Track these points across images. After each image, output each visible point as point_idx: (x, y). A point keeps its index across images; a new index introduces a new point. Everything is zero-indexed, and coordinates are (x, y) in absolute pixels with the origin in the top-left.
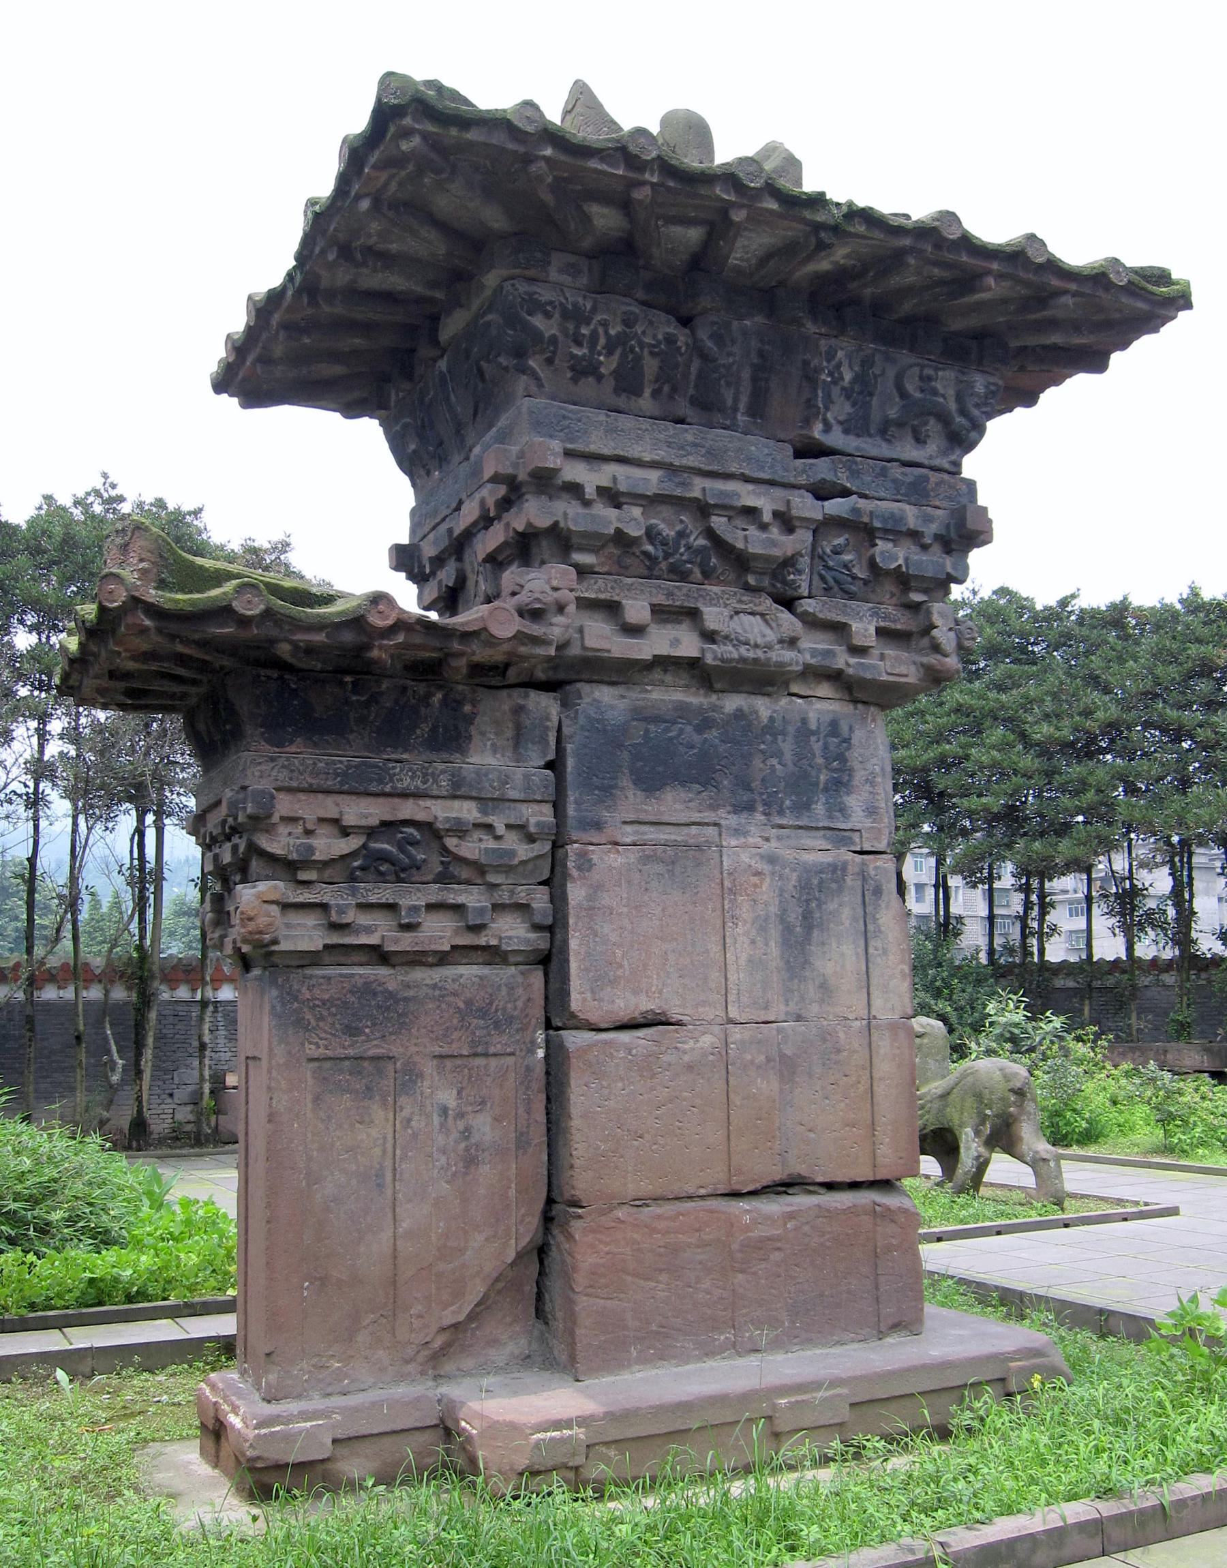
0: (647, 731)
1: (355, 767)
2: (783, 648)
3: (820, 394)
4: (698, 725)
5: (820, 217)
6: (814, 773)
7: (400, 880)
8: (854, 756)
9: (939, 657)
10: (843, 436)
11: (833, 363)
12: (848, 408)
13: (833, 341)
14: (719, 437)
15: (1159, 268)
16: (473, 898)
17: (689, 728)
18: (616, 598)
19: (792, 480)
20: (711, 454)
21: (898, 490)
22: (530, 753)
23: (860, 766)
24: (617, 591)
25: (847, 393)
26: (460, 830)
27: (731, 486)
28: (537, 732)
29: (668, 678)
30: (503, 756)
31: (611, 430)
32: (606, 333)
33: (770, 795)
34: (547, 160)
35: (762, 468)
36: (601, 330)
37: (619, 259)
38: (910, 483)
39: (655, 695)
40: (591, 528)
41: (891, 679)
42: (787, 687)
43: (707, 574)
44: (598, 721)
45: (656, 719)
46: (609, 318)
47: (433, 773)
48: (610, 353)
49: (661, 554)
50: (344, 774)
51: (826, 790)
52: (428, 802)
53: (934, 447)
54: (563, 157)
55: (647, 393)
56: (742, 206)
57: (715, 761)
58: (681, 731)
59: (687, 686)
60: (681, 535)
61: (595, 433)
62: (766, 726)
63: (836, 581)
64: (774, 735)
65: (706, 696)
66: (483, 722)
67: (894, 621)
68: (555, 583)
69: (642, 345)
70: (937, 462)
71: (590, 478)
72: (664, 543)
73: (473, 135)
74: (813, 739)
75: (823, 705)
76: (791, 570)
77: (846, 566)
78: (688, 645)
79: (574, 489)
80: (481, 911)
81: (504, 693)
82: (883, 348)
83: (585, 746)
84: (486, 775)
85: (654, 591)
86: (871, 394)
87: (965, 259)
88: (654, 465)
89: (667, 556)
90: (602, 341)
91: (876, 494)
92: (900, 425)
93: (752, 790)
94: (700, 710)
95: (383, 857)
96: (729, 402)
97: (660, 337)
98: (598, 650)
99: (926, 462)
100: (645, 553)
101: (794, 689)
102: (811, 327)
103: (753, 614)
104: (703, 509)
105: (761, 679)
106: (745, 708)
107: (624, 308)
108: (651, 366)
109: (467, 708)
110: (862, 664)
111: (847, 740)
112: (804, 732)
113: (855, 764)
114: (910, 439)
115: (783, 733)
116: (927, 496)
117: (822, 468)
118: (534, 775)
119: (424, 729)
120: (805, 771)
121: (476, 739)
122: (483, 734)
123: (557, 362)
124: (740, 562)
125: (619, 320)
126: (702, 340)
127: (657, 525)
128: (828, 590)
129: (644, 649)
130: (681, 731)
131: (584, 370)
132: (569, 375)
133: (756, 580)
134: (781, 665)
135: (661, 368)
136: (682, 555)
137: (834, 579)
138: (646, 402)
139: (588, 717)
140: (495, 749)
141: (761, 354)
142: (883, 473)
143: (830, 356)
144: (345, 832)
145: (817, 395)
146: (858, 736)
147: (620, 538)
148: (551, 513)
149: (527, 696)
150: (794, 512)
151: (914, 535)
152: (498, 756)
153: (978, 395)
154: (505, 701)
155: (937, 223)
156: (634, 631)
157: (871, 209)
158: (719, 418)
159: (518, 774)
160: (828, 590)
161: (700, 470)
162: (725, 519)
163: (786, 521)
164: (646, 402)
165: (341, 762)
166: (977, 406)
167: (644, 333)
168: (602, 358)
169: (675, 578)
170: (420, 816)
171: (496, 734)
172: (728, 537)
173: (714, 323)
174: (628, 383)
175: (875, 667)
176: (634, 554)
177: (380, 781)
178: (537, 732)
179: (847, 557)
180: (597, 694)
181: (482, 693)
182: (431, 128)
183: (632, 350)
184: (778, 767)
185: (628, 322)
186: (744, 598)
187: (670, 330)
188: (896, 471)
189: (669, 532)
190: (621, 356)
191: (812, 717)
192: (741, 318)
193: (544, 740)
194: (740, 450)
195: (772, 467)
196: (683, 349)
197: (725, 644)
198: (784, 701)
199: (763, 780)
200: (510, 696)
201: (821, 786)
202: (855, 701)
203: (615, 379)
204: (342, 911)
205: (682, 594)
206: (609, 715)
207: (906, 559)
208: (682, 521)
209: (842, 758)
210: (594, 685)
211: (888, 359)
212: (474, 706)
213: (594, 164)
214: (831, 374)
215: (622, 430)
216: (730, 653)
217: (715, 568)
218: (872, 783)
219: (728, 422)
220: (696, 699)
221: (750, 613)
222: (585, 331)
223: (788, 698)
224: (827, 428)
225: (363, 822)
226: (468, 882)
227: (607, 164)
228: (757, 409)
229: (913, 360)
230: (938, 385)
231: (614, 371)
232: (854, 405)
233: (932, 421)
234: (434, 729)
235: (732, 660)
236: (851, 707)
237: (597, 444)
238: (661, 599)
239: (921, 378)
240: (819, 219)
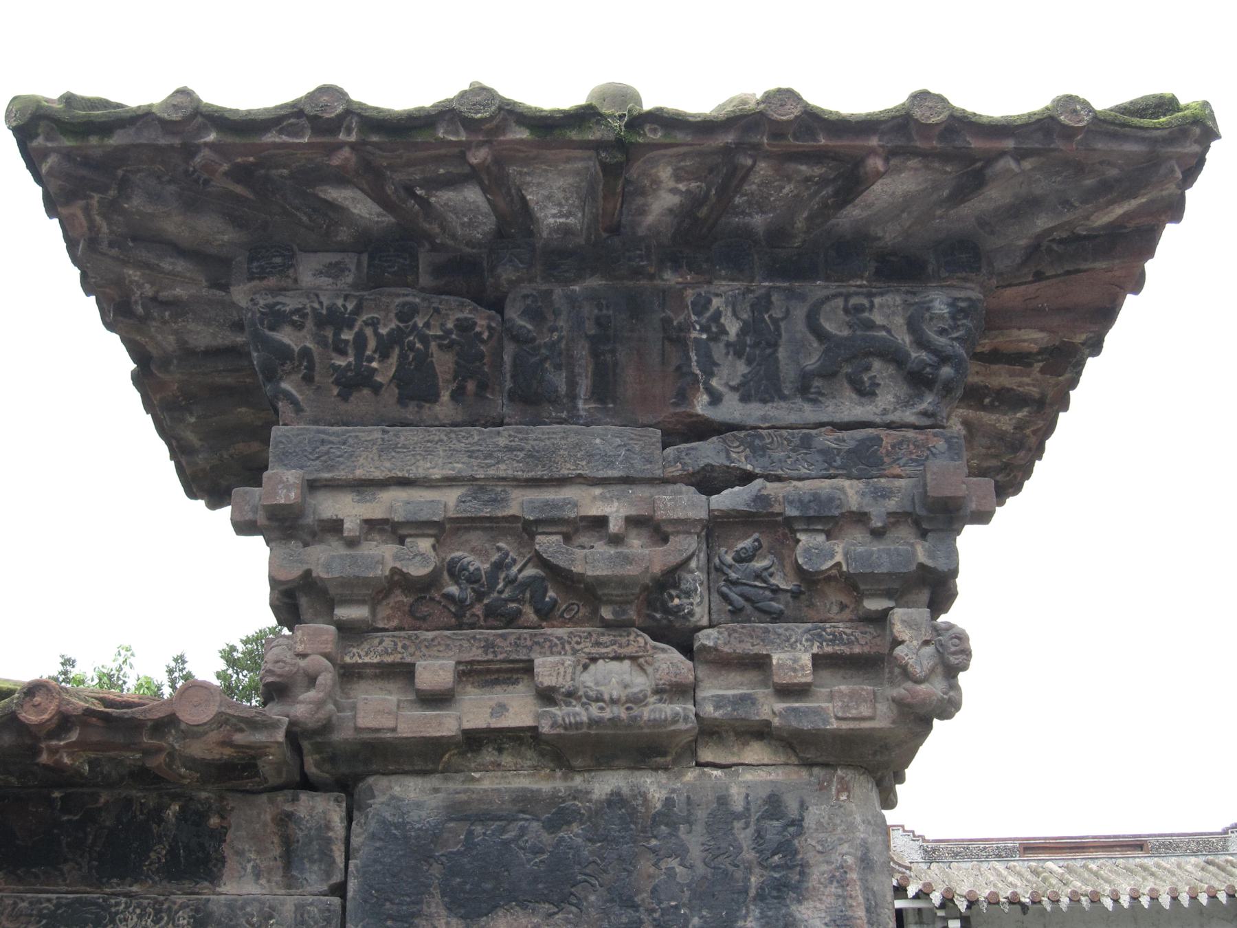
0: (470, 833)
1: (67, 905)
2: (660, 701)
3: (694, 358)
4: (549, 820)
5: (595, 134)
6: (739, 874)
8: (809, 845)
9: (909, 684)
10: (740, 406)
11: (708, 315)
12: (742, 368)
13: (703, 290)
15: (1154, 96)
17: (535, 825)
18: (408, 660)
19: (658, 473)
20: (533, 457)
21: (830, 463)
22: (307, 875)
23: (820, 858)
24: (412, 650)
25: (737, 349)
27: (568, 493)
28: (315, 846)
29: (506, 759)
30: (269, 881)
31: (386, 449)
32: (376, 333)
33: (664, 912)
34: (210, 145)
35: (610, 464)
36: (369, 332)
38: (849, 451)
39: (486, 784)
40: (350, 572)
41: (845, 726)
42: (694, 753)
43: (546, 613)
44: (397, 826)
45: (483, 817)
47: (169, 908)
48: (384, 356)
49: (470, 594)
51: (761, 897)
53: (890, 398)
54: (230, 139)
55: (445, 396)
56: (480, 145)
57: (577, 868)
58: (523, 830)
59: (535, 768)
60: (499, 566)
61: (364, 454)
62: (659, 813)
63: (747, 599)
64: (673, 826)
65: (565, 778)
66: (237, 839)
67: (850, 643)
68: (300, 648)
69: (425, 340)
70: (895, 417)
71: (350, 510)
72: (473, 579)
73: (116, 140)
74: (738, 825)
75: (755, 773)
76: (674, 593)
77: (758, 576)
78: (518, 709)
79: (335, 527)
82: (786, 284)
83: (376, 861)
84: (243, 908)
85: (466, 644)
86: (774, 345)
87: (823, 142)
88: (450, 481)
89: (480, 596)
90: (372, 344)
91: (794, 473)
92: (829, 374)
93: (635, 907)
94: (554, 798)
96: (563, 389)
97: (450, 325)
98: (378, 730)
99: (878, 420)
100: (449, 597)
101: (706, 755)
103: (618, 658)
104: (527, 529)
105: (645, 749)
106: (625, 791)
107: (398, 301)
108: (443, 362)
109: (214, 821)
110: (794, 710)
111: (798, 823)
112: (723, 815)
113: (812, 857)
114: (848, 392)
115: (689, 821)
116: (879, 463)
117: (708, 452)
118: (311, 904)
119: (159, 852)
120: (726, 873)
121: (232, 863)
122: (240, 853)
123: (317, 379)
124: (586, 593)
125: (392, 315)
126: (510, 320)
127: (460, 559)
128: (736, 612)
129: (446, 724)
130: (523, 830)
131: (355, 381)
132: (336, 391)
133: (615, 613)
134: (656, 723)
135: (457, 363)
136: (501, 592)
137: (742, 595)
138: (445, 407)
139: (383, 822)
140: (257, 875)
141: (598, 322)
142: (806, 443)
143: (701, 305)
145: (689, 359)
146: (815, 814)
147: (399, 581)
148: (301, 562)
149: (295, 799)
150: (660, 514)
151: (860, 518)
152: (263, 881)
153: (941, 317)
154: (264, 811)
155: (762, 106)
156: (437, 699)
157: (660, 110)
158: (550, 410)
159: (289, 904)
161: (515, 479)
162: (559, 537)
163: (654, 528)
164: (445, 407)
165: (49, 900)
166: (942, 332)
167: (427, 325)
168: (374, 365)
169: (496, 623)
171: (258, 852)
172: (561, 561)
173: (525, 297)
174: (416, 388)
175: (816, 712)
176: (432, 599)
178: (315, 846)
179: (758, 564)
180: (397, 790)
181: (232, 801)
182: (68, 143)
183: (411, 347)
184: (679, 869)
185: (407, 314)
186: (604, 639)
187: (466, 314)
188: (827, 439)
189: (479, 564)
190: (400, 357)
191: (735, 791)
192: (567, 282)
193: (325, 855)
194: (577, 446)
195: (627, 458)
196: (485, 335)
197: (568, 704)
198: (691, 776)
199: (654, 891)
200: (271, 801)
201: (752, 892)
202: (809, 764)
203: (398, 386)
205: (506, 643)
206: (414, 816)
207: (846, 554)
208: (499, 549)
209: (786, 848)
210: (393, 778)
211: (791, 295)
212: (223, 818)
213: (271, 138)
215: (404, 447)
216: (575, 714)
217: (554, 603)
218: (843, 883)
219: (564, 415)
220: (547, 784)
221: (613, 659)
222: (347, 336)
223: (698, 770)
224: (716, 399)
227: (288, 135)
228: (604, 390)
229: (833, 288)
230: (878, 319)
231: (394, 377)
232: (749, 362)
233: (877, 364)
234: (173, 852)
235: (578, 725)
236: (804, 773)
237: (366, 468)
238: (476, 654)
239: (846, 311)
240: (591, 137)
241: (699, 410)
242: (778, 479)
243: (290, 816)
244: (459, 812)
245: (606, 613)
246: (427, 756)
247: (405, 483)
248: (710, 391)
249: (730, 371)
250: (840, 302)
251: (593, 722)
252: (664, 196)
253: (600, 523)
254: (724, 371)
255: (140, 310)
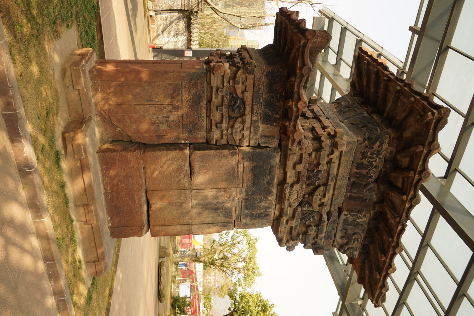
7: (229, 106)
13: (368, 217)
14: (344, 189)
16: (225, 125)
21: (329, 232)
25: (354, 220)
26: (243, 122)
27: (331, 191)
29: (281, 175)
36: (374, 160)
37: (393, 164)
39: (277, 171)
41: (280, 230)
46: (378, 162)
48: (368, 162)
50: (258, 92)
52: (250, 114)
55: (357, 171)
65: (276, 184)
66: (271, 128)
69: (370, 170)
70: (336, 242)
72: (317, 175)
80: (221, 128)
81: (279, 133)
86: (354, 226)
88: (338, 173)
90: (371, 160)
95: (236, 102)
96: (353, 191)
100: (314, 170)
101: (277, 206)
102: (372, 212)
103: (297, 196)
104: (325, 184)
107: (380, 166)
108: (364, 172)
109: (275, 124)
111: (264, 218)
113: (257, 221)
114: (342, 235)
116: (327, 239)
122: (268, 128)
124: (311, 194)
131: (364, 155)
138: (355, 170)
139: (271, 155)
142: (333, 229)
143: (365, 216)
144: (243, 92)
149: (278, 139)
151: (317, 236)
154: (277, 134)
156: (294, 167)
160: (303, 215)
163: (322, 205)
164: (355, 170)
170: (246, 112)
173: (375, 188)
174: (360, 166)
177: (256, 102)
181: (278, 128)
183: (368, 168)
187: (373, 177)
188: (333, 232)
191: (270, 210)
192: (376, 195)
193: (265, 143)
198: (274, 203)
204: (222, 91)
206: (272, 160)
207: (310, 234)
209: (259, 217)
211: (363, 231)
214: (360, 216)
222: (374, 156)
224: (345, 215)
225: (245, 97)
226: (228, 124)
228: (351, 198)
233: (346, 241)
234: (269, 115)
239: (358, 239)
241: (344, 212)
242: (327, 224)
243: (274, 138)
244: (272, 167)
245: (306, 196)
246: (284, 164)
247: (339, 165)
248: (347, 215)
249: (350, 219)
250: (360, 238)
251: (285, 194)
252: (395, 197)
253: (324, 196)
254: (351, 217)
255: (397, 95)
